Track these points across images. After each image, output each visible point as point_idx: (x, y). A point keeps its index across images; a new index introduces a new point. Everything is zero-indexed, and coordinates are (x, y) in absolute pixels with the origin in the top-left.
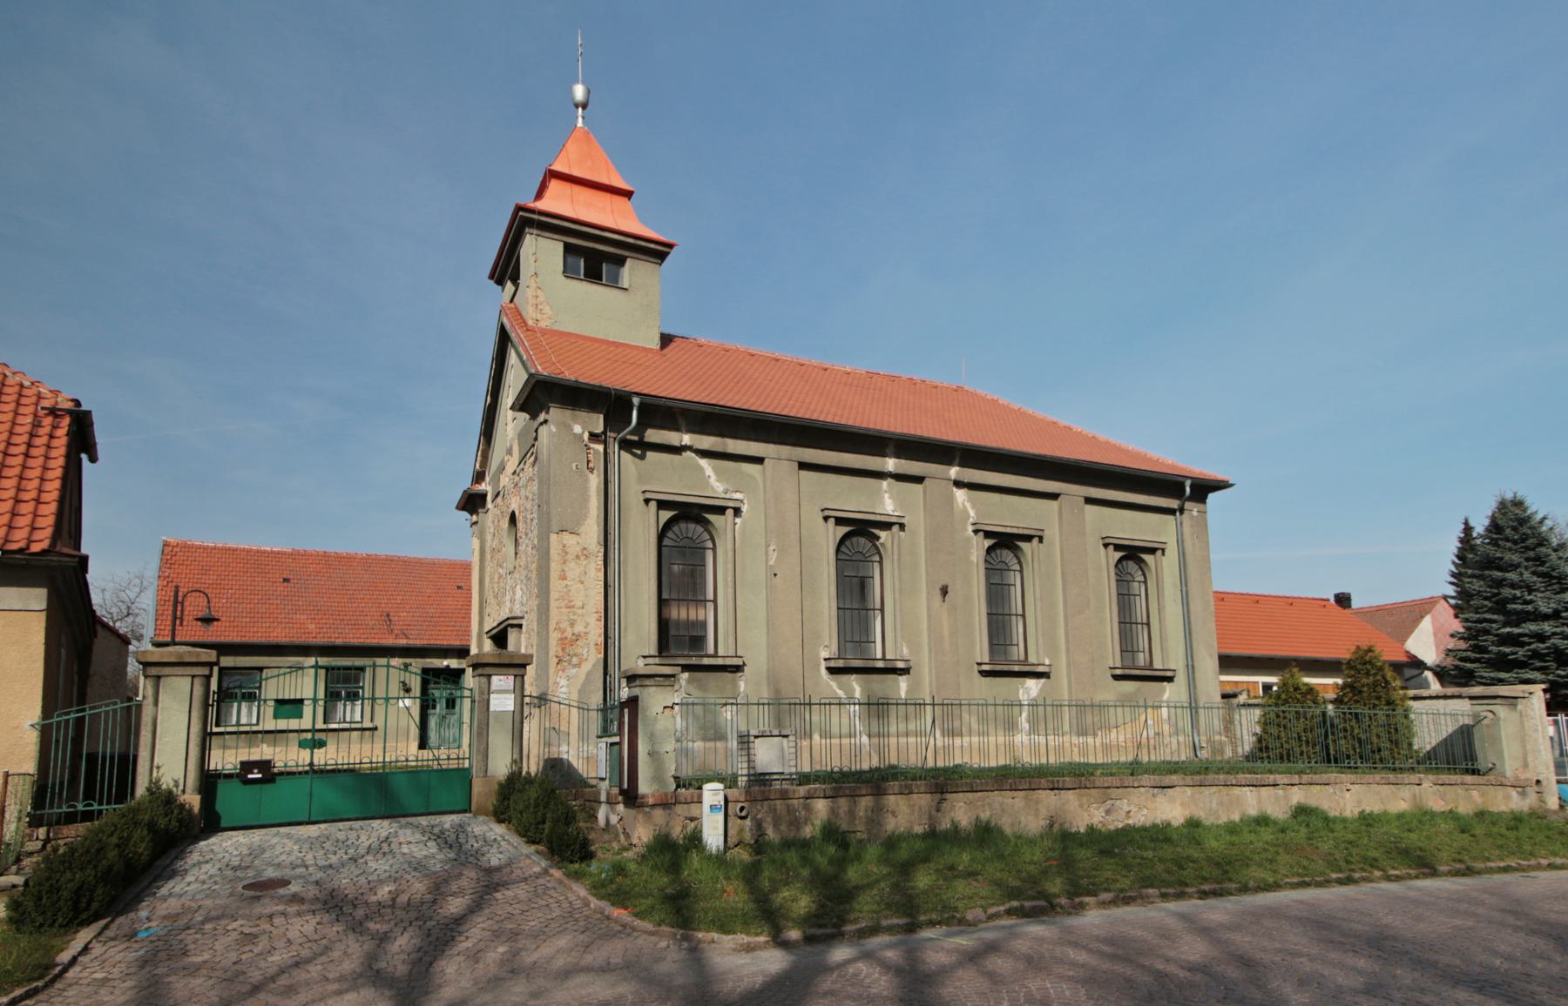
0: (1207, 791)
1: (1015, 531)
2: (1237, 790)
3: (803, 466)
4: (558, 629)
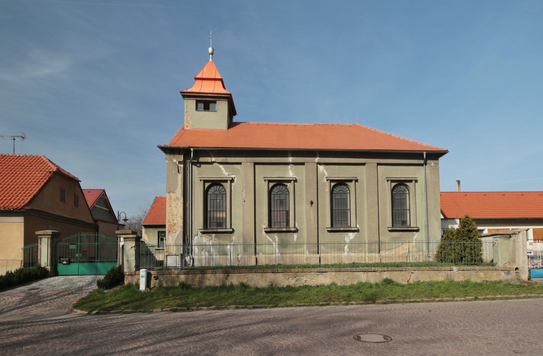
0: (342, 274)
1: (344, 179)
2: (357, 273)
3: (379, 164)
4: (169, 222)
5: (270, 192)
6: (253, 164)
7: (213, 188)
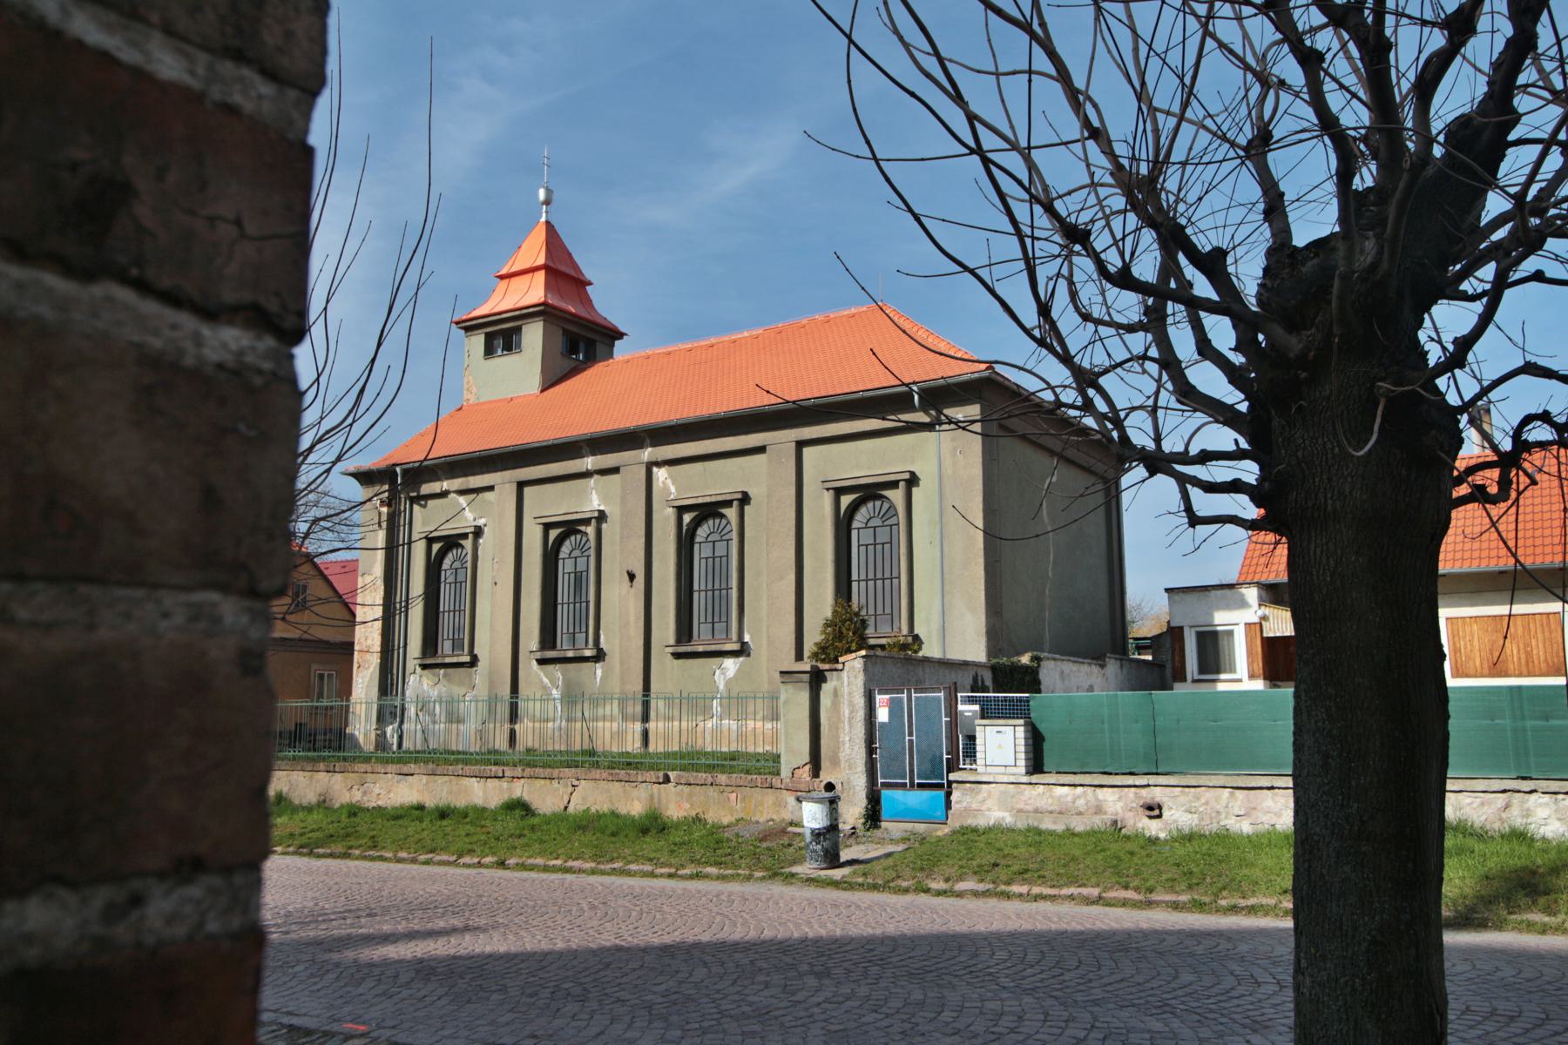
0: (441, 780)
1: (714, 499)
2: (466, 781)
6: (514, 486)
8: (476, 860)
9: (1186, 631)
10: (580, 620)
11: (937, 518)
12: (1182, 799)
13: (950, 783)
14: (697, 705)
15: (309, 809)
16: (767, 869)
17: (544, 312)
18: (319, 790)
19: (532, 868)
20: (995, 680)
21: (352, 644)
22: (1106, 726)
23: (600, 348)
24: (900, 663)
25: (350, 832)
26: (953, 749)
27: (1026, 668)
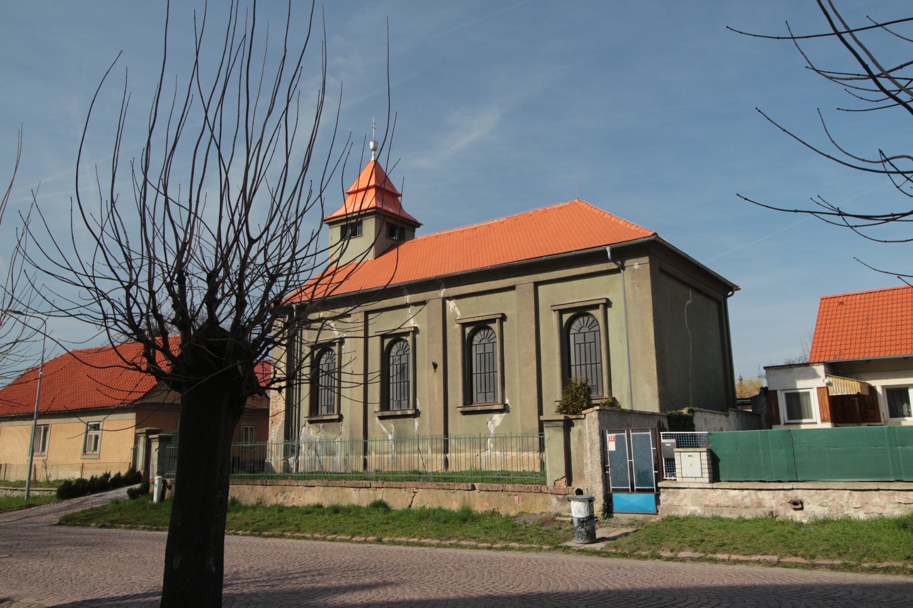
0: (332, 489)
1: (484, 318)
2: (347, 490)
5: (565, 333)
6: (363, 314)
7: (577, 322)
8: (363, 539)
9: (779, 393)
10: (404, 392)
11: (624, 326)
12: (816, 497)
13: (658, 489)
14: (479, 442)
15: (254, 508)
16: (551, 544)
17: (375, 212)
18: (257, 496)
19: (399, 543)
20: (669, 423)
21: (268, 410)
22: (761, 451)
23: (407, 233)
24: (615, 417)
25: (283, 521)
26: (658, 466)
27: (686, 417)
